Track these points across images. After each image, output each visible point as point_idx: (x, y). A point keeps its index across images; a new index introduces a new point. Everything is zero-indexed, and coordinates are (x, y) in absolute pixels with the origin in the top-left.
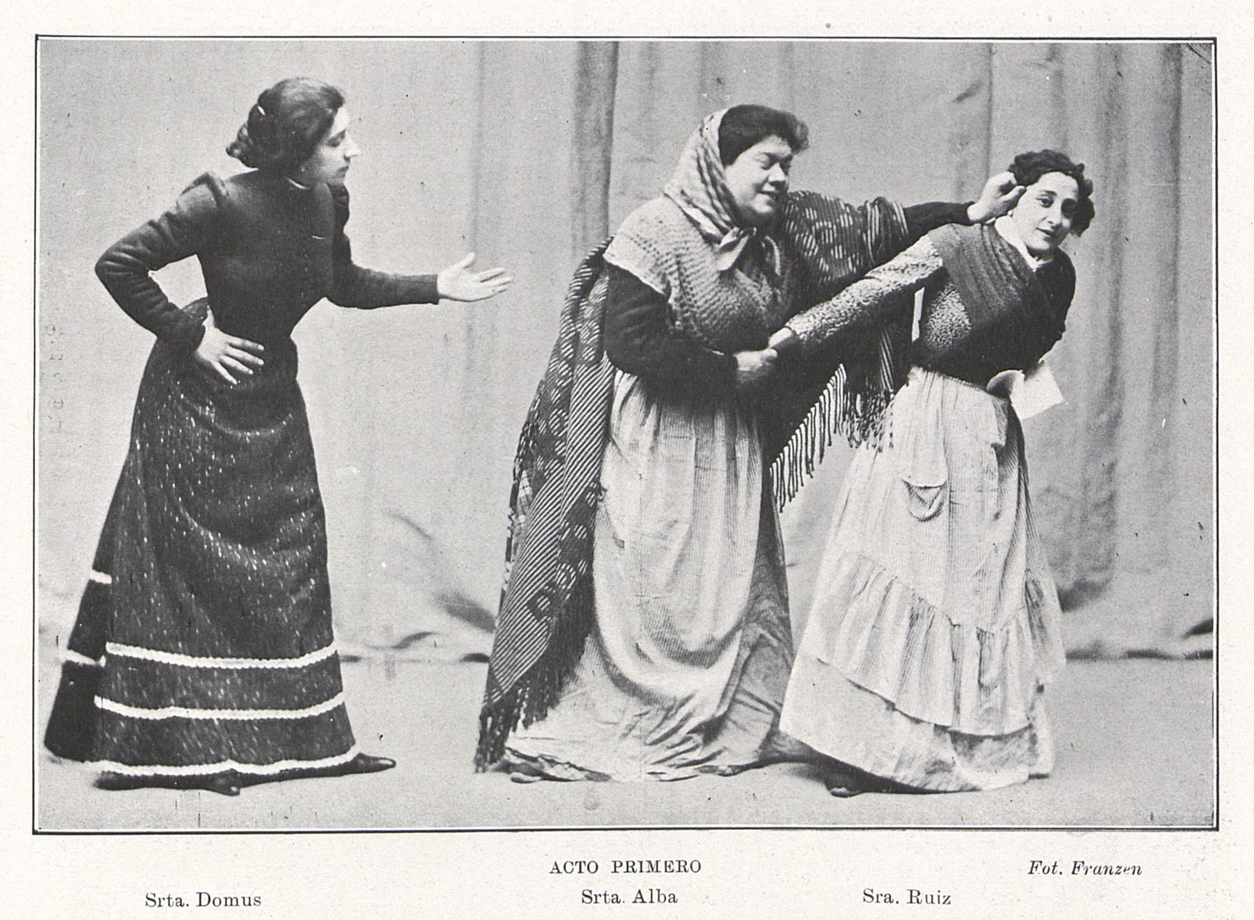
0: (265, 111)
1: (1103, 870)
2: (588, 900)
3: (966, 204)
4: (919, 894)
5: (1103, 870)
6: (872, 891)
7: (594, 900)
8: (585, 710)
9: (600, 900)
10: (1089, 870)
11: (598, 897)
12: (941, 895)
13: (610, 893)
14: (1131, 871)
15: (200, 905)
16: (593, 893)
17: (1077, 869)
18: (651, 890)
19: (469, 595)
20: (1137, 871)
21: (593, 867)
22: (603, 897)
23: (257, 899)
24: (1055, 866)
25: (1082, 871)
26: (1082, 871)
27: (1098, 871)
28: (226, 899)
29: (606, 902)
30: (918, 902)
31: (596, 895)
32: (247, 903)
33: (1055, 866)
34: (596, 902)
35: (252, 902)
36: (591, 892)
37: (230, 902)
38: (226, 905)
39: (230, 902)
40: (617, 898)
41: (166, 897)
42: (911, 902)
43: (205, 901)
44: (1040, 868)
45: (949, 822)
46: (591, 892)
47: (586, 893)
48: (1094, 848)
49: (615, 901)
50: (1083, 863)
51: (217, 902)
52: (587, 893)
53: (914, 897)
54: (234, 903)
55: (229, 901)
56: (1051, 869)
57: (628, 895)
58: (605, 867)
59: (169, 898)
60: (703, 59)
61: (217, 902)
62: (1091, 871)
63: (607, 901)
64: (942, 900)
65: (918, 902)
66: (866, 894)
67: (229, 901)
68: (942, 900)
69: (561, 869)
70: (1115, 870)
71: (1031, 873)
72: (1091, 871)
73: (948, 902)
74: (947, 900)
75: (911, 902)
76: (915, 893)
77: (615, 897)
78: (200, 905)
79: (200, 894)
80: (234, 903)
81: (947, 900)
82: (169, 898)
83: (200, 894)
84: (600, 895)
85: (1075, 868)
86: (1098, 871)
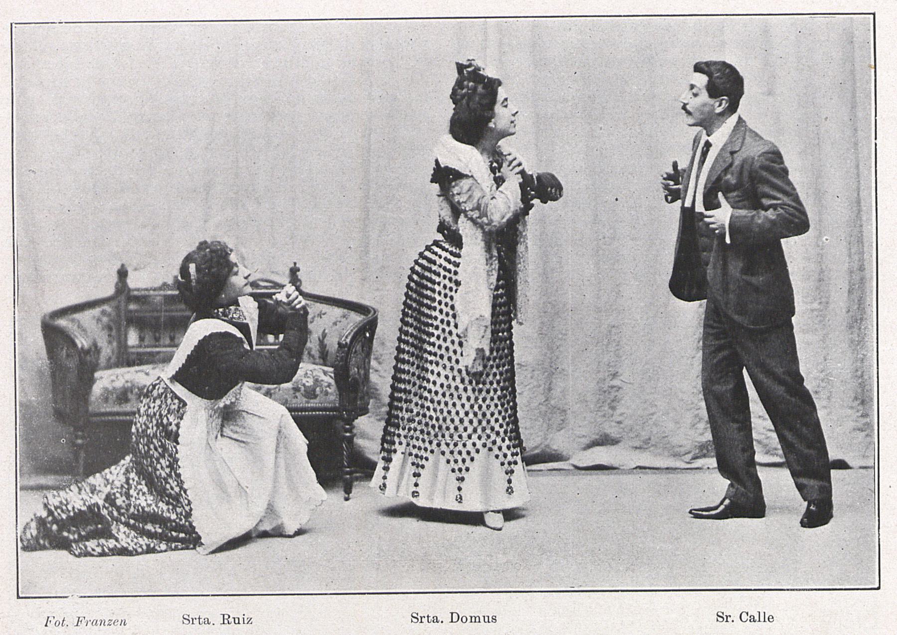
0: (537, 183)
1: (99, 623)
4: (229, 617)
5: (99, 623)
6: (717, 620)
7: (725, 620)
9: (196, 622)
10: (89, 622)
11: (194, 620)
13: (431, 616)
14: (119, 623)
15: (452, 622)
16: (725, 614)
17: (80, 622)
18: (759, 612)
19: (381, 505)
22: (198, 620)
23: (494, 618)
24: (63, 621)
27: (95, 623)
28: (471, 617)
29: (428, 622)
30: (229, 623)
31: (726, 616)
32: (486, 620)
33: (63, 621)
34: (421, 622)
35: (490, 619)
36: (723, 613)
38: (471, 622)
40: (754, 618)
41: (197, 617)
42: (224, 623)
43: (455, 618)
48: (234, 608)
49: (206, 622)
50: (84, 618)
51: (464, 620)
54: (477, 620)
55: (473, 618)
57: (71, 620)
59: (199, 618)
60: (486, 40)
61: (464, 620)
62: (90, 623)
63: (430, 621)
65: (229, 623)
67: (473, 618)
68: (246, 622)
70: (106, 623)
71: (77, 625)
73: (250, 622)
74: (494, 619)
75: (224, 623)
76: (226, 617)
77: (206, 620)
78: (452, 622)
79: (452, 614)
80: (477, 620)
81: (250, 621)
82: (428, 617)
84: (424, 617)
85: (78, 621)
86: (95, 623)
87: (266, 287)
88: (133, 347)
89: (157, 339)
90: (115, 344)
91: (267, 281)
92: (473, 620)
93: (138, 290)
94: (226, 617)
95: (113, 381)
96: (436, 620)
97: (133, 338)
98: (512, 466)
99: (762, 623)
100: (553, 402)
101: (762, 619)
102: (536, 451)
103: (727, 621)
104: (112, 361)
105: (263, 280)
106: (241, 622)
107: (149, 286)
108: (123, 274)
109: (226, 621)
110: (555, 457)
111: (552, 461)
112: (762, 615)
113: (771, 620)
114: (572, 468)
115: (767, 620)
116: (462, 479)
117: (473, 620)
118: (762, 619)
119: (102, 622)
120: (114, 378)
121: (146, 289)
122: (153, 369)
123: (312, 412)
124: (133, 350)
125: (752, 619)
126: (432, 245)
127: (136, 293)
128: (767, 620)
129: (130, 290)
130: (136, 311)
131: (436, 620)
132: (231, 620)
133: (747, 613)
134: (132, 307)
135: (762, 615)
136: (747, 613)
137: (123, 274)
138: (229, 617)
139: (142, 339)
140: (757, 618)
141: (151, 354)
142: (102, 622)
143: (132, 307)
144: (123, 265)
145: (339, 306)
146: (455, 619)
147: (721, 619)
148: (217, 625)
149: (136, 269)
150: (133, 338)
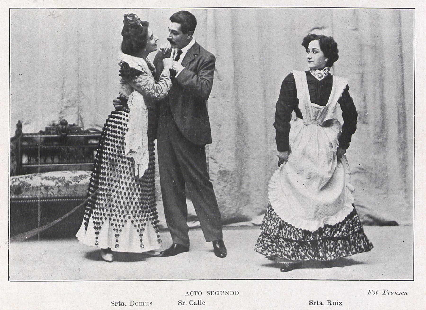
2: (311, 304)
3: (343, 94)
4: (331, 302)
5: (394, 293)
7: (313, 304)
8: (150, 246)
12: (339, 302)
13: (319, 302)
14: (404, 293)
15: (131, 305)
16: (115, 302)
20: (406, 293)
21: (200, 294)
22: (118, 303)
24: (377, 292)
25: (387, 293)
26: (387, 293)
33: (377, 292)
36: (312, 301)
37: (141, 304)
39: (141, 304)
41: (316, 301)
43: (132, 304)
44: (372, 293)
45: (135, 278)
46: (312, 301)
47: (311, 301)
51: (137, 304)
52: (311, 301)
53: (329, 303)
54: (143, 304)
55: (141, 303)
56: (376, 292)
58: (204, 293)
59: (119, 303)
61: (137, 304)
62: (390, 293)
64: (339, 304)
66: (310, 302)
67: (141, 303)
69: (189, 294)
70: (398, 293)
71: (384, 294)
72: (390, 293)
74: (341, 304)
76: (329, 302)
78: (131, 305)
79: (131, 301)
80: (143, 304)
82: (317, 302)
83: (131, 301)
87: (93, 133)
88: (25, 164)
89: (45, 160)
90: (15, 163)
91: (95, 130)
92: (141, 304)
93: (27, 134)
94: (329, 302)
95: (13, 182)
96: (321, 304)
97: (25, 160)
98: (143, 227)
99: (337, 306)
100: (242, 191)
101: (200, 303)
102: (234, 217)
103: (183, 305)
104: (14, 172)
105: (92, 130)
106: (337, 304)
107: (33, 132)
108: (19, 126)
109: (329, 304)
110: (245, 219)
111: (241, 222)
112: (200, 301)
113: (204, 304)
114: (253, 225)
115: (202, 304)
116: (118, 235)
117: (141, 304)
118: (200, 303)
119: (396, 293)
120: (14, 180)
121: (31, 134)
122: (34, 176)
123: (57, 199)
124: (25, 166)
125: (195, 304)
126: (109, 118)
127: (26, 136)
128: (202, 304)
129: (23, 134)
130: (26, 146)
131: (321, 304)
132: (332, 303)
133: (193, 301)
134: (25, 143)
135: (200, 301)
136: (193, 301)
137: (19, 126)
138: (331, 302)
139: (29, 160)
140: (197, 303)
141: (33, 168)
142: (396, 293)
143: (25, 143)
144: (19, 121)
145: (288, 127)
146: (132, 304)
147: (181, 304)
148: (325, 305)
149: (26, 124)
150: (25, 160)
